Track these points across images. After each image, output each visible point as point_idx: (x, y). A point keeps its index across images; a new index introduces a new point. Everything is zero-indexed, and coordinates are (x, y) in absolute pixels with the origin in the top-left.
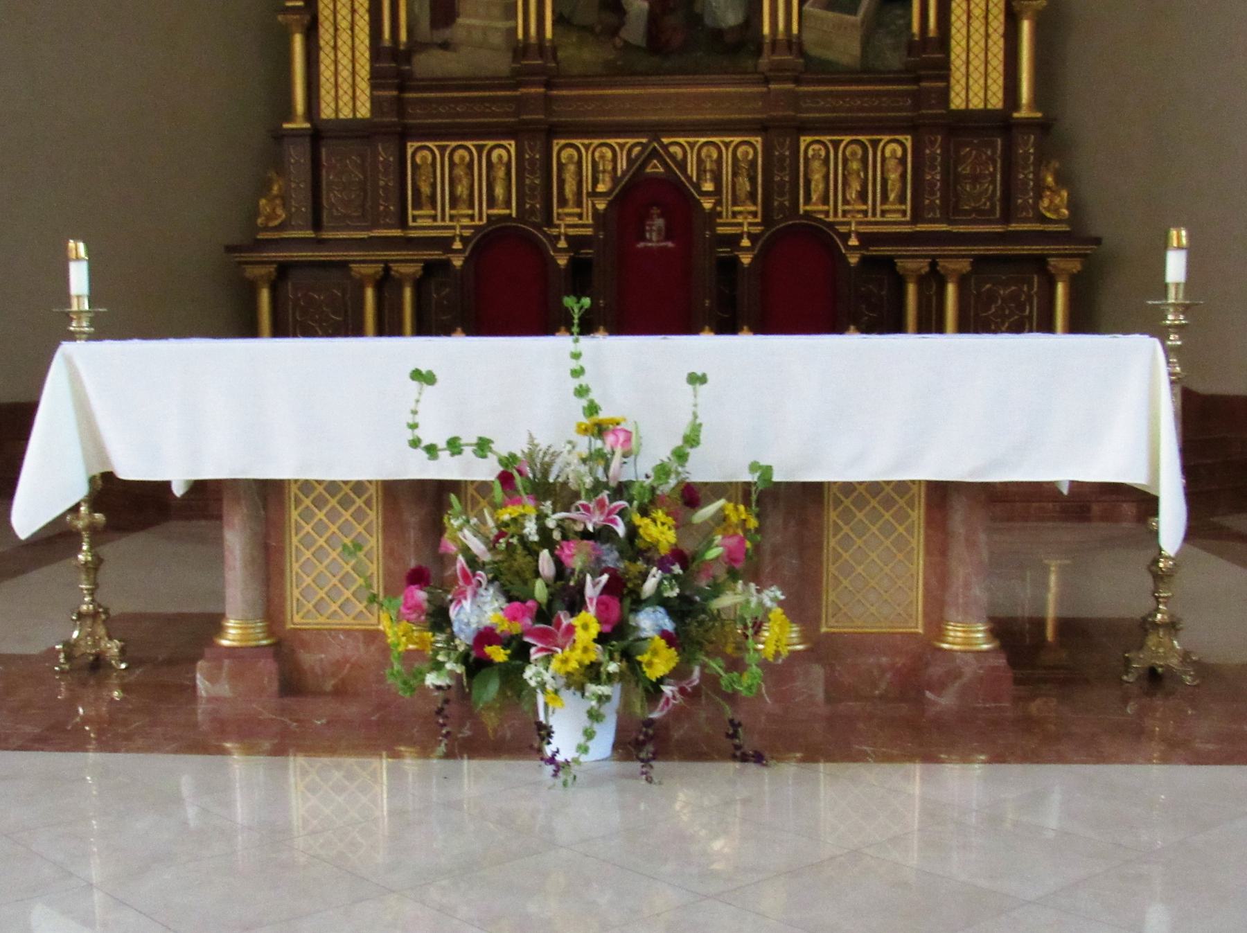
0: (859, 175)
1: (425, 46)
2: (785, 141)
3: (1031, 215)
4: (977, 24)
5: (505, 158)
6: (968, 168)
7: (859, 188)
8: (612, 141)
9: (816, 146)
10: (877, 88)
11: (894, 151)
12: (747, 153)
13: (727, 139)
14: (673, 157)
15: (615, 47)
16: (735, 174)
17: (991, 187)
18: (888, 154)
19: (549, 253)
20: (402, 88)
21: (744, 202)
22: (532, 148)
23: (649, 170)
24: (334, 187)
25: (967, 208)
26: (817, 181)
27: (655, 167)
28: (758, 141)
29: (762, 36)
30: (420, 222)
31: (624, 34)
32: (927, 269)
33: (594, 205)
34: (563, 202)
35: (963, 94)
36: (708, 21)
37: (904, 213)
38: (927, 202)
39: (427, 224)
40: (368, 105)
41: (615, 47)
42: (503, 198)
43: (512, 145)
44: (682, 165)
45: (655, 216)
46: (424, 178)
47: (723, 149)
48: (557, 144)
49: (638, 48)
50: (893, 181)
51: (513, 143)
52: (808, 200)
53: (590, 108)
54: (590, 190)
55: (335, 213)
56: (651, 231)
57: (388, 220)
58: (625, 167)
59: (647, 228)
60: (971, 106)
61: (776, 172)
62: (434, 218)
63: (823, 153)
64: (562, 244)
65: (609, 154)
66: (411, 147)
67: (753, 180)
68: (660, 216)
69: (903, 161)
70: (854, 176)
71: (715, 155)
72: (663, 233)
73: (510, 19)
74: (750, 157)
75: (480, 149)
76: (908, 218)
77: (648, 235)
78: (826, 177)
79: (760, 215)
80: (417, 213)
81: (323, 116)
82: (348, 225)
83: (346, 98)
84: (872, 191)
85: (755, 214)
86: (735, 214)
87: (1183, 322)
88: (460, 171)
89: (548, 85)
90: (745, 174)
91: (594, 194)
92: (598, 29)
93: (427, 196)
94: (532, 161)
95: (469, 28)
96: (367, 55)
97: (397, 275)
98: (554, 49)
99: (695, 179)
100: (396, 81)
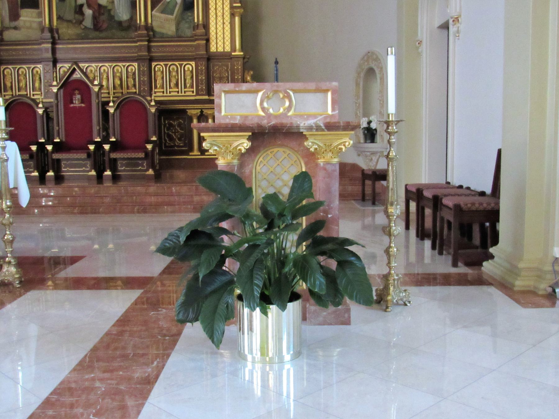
1: (8, 28)
2: (145, 64)
3: (204, 93)
4: (220, 19)
5: (191, 69)
10: (83, 46)
13: (124, 64)
16: (127, 77)
18: (186, 69)
22: (143, 66)
29: (137, 24)
31: (84, 23)
35: (215, 46)
36: (116, 19)
37: (193, 92)
39: (106, 96)
43: (193, 64)
45: (77, 94)
47: (123, 67)
48: (193, 63)
49: (90, 29)
53: (123, 51)
56: (75, 100)
59: (74, 99)
61: (141, 76)
62: (178, 92)
63: (161, 69)
64: (153, 103)
66: (154, 64)
67: (134, 80)
68: (79, 94)
72: (80, 101)
73: (40, 18)
74: (134, 71)
76: (195, 94)
77: (74, 102)
78: (163, 78)
79: (195, 92)
81: (211, 51)
87: (5, 137)
92: (74, 21)
95: (25, 21)
100: (147, 38)
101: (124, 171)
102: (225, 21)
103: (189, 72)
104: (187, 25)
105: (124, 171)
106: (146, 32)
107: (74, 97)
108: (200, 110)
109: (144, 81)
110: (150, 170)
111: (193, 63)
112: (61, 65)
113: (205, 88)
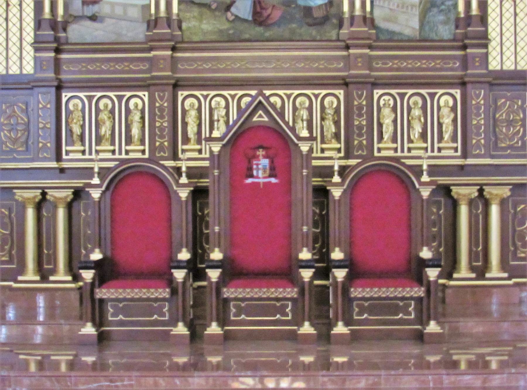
0: (420, 120)
1: (77, 18)
6: (504, 115)
7: (420, 131)
8: (225, 93)
9: (387, 98)
11: (447, 102)
12: (332, 103)
13: (316, 92)
14: (273, 106)
15: (227, 19)
16: (323, 119)
17: (522, 130)
18: (442, 103)
19: (173, 188)
20: (58, 51)
21: (331, 141)
22: (162, 99)
23: (255, 119)
24: (4, 127)
25: (503, 145)
26: (388, 125)
27: (260, 116)
28: (340, 93)
30: (72, 156)
31: (233, 9)
32: (476, 194)
33: (210, 148)
34: (186, 140)
35: (498, 58)
37: (456, 149)
38: (474, 141)
40: (32, 63)
41: (227, 19)
42: (139, 137)
43: (145, 95)
44: (282, 115)
45: (261, 157)
46: (75, 121)
50: (447, 124)
51: (146, 93)
52: (381, 138)
54: (208, 136)
55: (4, 148)
56: (258, 169)
57: (45, 154)
58: (235, 117)
59: (255, 167)
60: (505, 68)
62: (83, 152)
63: (392, 102)
65: (223, 103)
66: (65, 95)
68: (265, 157)
69: (454, 109)
70: (417, 121)
71: (307, 104)
72: (268, 172)
74: (335, 105)
75: (120, 98)
76: (459, 153)
77: (255, 173)
80: (69, 148)
82: (15, 157)
83: (14, 58)
84: (432, 133)
85: (339, 150)
86: (323, 150)
88: (104, 116)
89: (174, 49)
90: (331, 118)
91: (210, 139)
92: (214, 6)
93: (78, 136)
94: (161, 109)
96: (32, 24)
97: (52, 199)
98: (180, 22)
99: (291, 124)
101: (121, 323)
102: (518, 11)
103: (390, 109)
104: (441, 18)
105: (121, 323)
106: (52, 33)
107: (255, 162)
108: (40, 191)
109: (162, 129)
110: (180, 324)
111: (456, 93)
112: (70, 95)
113: (169, 144)
